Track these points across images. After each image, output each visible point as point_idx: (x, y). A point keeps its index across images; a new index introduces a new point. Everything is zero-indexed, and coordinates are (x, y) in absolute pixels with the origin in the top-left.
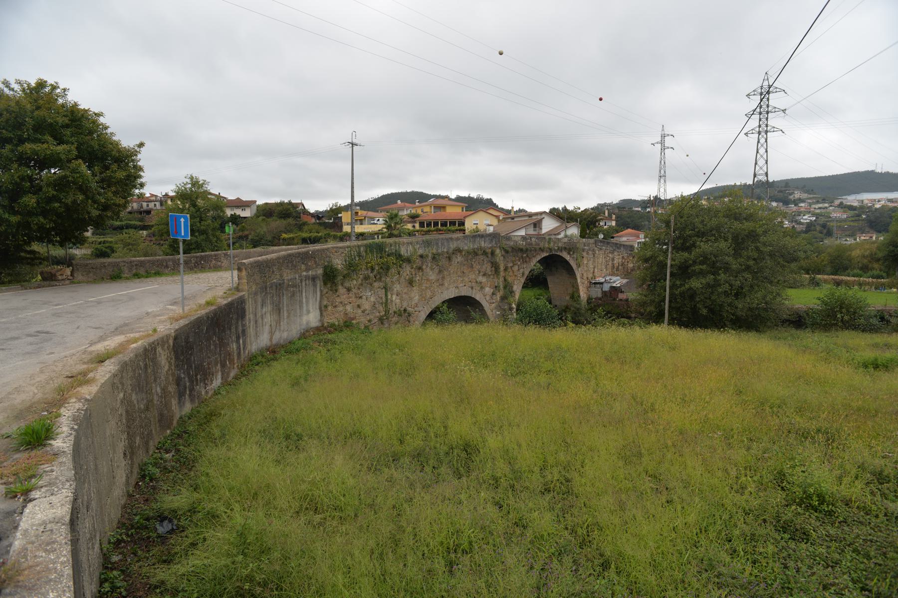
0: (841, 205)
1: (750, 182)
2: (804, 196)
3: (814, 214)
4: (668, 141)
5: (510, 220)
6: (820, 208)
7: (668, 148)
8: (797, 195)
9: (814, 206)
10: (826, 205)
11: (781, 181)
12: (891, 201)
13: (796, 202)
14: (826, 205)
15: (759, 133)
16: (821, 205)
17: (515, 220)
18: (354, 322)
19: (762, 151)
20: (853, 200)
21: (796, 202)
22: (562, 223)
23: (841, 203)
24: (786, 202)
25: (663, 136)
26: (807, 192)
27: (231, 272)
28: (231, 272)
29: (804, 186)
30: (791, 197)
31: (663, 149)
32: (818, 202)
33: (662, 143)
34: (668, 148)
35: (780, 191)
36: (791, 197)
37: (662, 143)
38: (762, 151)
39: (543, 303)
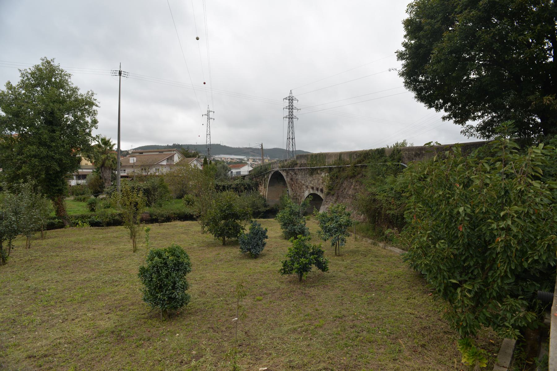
5: (158, 153)
7: (211, 118)
12: (231, 159)
17: (144, 154)
23: (214, 159)
25: (209, 112)
33: (208, 115)
34: (211, 118)
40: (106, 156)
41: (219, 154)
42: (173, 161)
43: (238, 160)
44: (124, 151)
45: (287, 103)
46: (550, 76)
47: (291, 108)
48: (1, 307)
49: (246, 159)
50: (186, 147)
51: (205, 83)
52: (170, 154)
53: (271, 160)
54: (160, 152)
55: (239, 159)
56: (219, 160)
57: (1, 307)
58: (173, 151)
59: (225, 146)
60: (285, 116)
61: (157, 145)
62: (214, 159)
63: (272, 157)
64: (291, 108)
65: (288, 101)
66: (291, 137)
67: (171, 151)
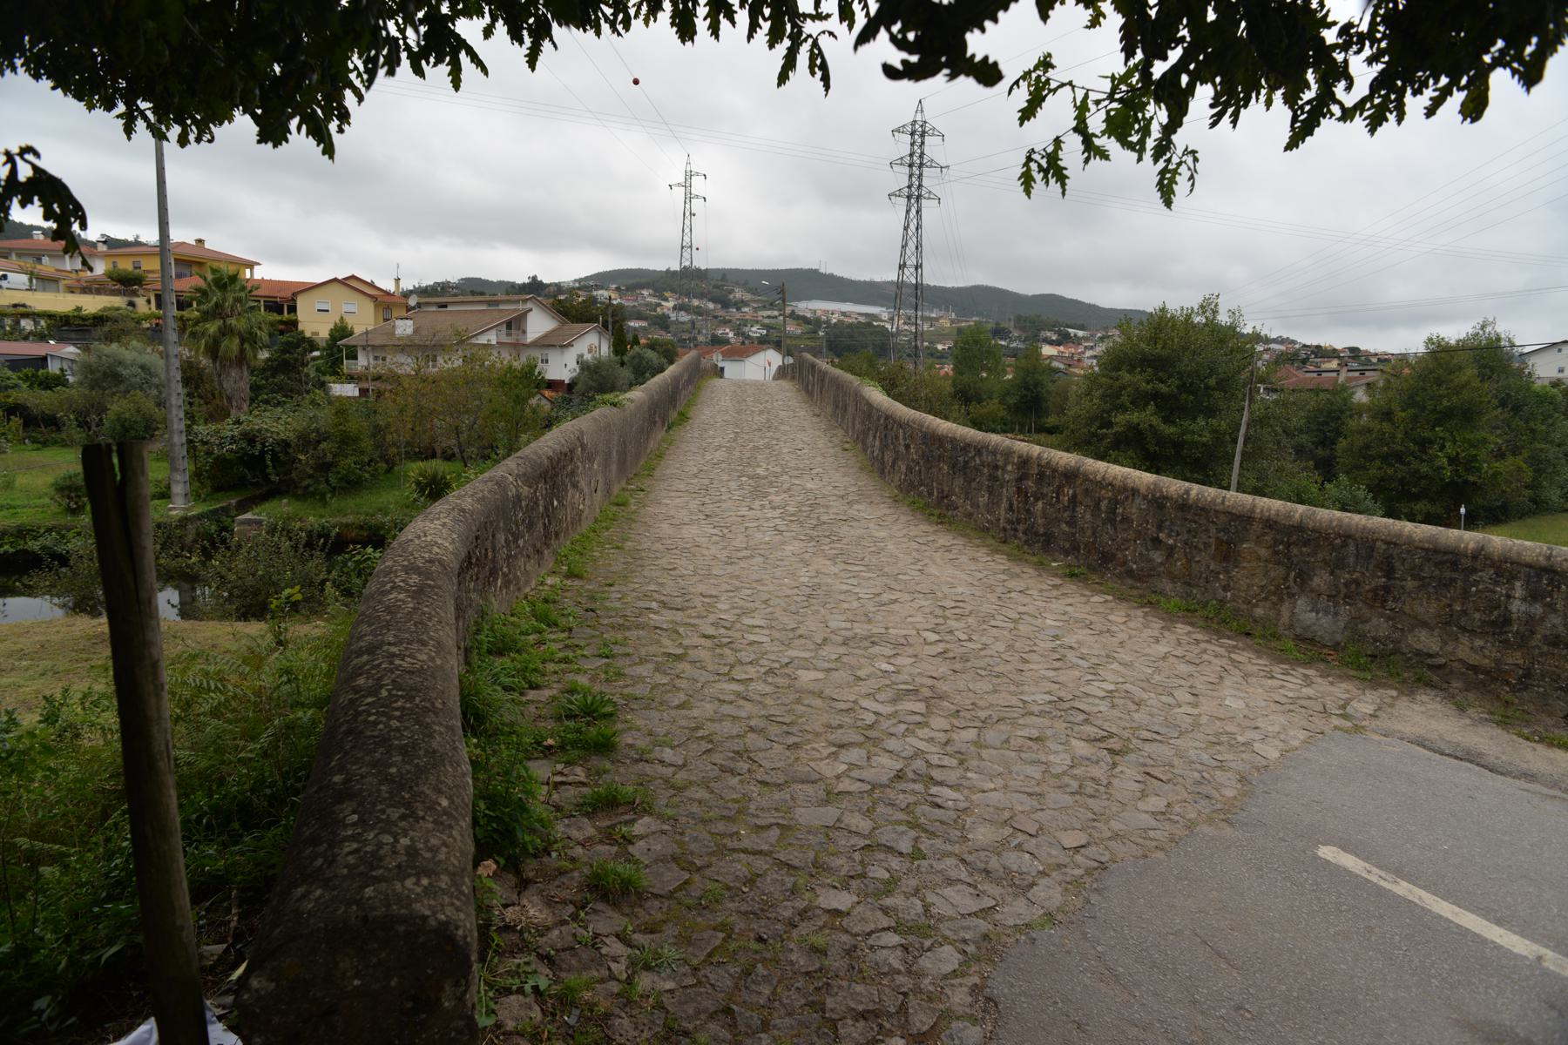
0: (793, 315)
1: (676, 267)
2: (748, 297)
3: (764, 326)
4: (698, 185)
5: (434, 309)
6: (769, 317)
7: (697, 197)
8: (738, 294)
9: (761, 313)
10: (776, 313)
11: (717, 271)
12: (844, 314)
13: (739, 304)
14: (776, 313)
15: (909, 197)
16: (769, 313)
17: (449, 308)
18: (176, 130)
19: (687, 230)
20: (806, 307)
21: (739, 304)
22: (563, 324)
23: (793, 312)
24: (726, 304)
25: (689, 175)
26: (750, 291)
27: (177, 235)
28: (177, 235)
29: (746, 283)
30: (731, 296)
31: (689, 197)
32: (764, 308)
33: (687, 185)
34: (697, 197)
35: (716, 287)
36: (731, 296)
37: (687, 185)
38: (687, 230)
39: (263, 676)
40: (219, 323)
41: (810, 298)
42: (524, 332)
43: (862, 319)
44: (550, 285)
45: (903, 145)
46: (1310, 57)
47: (916, 163)
48: (5, 681)
49: (885, 316)
50: (720, 277)
51: (636, 82)
52: (515, 310)
53: (959, 321)
54: (489, 303)
55: (866, 315)
56: (809, 315)
57: (5, 681)
58: (525, 301)
59: (831, 276)
60: (895, 188)
61: (644, 267)
62: (793, 312)
63: (964, 312)
64: (916, 163)
65: (908, 138)
66: (912, 261)
67: (517, 302)
